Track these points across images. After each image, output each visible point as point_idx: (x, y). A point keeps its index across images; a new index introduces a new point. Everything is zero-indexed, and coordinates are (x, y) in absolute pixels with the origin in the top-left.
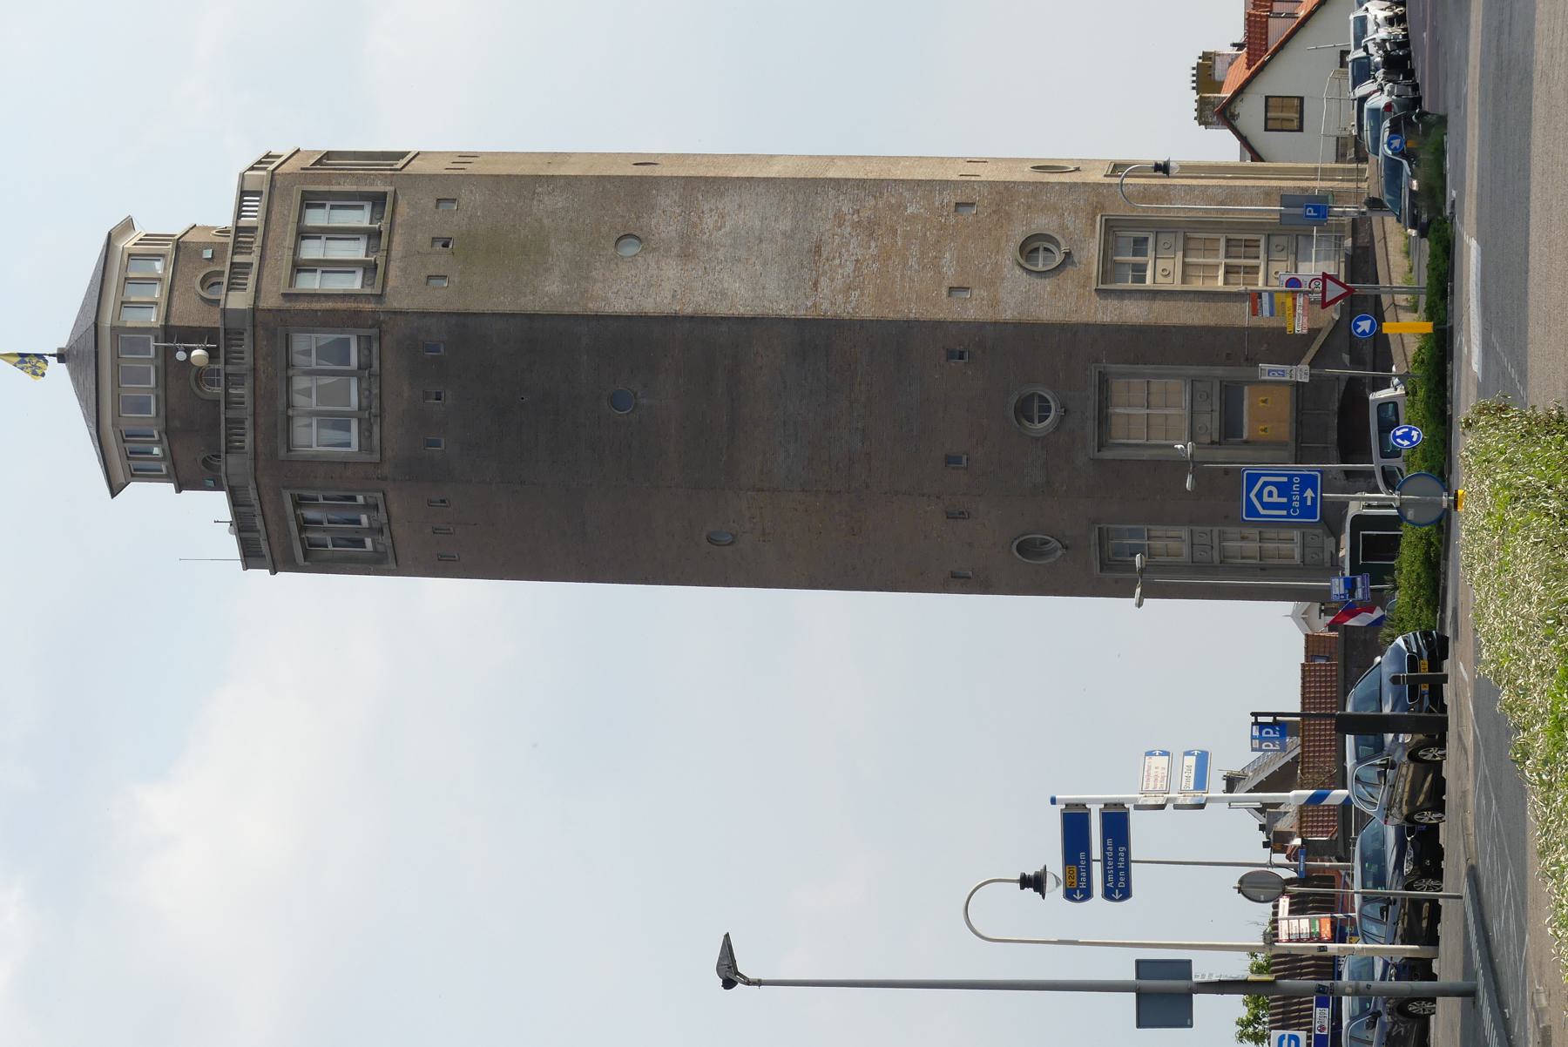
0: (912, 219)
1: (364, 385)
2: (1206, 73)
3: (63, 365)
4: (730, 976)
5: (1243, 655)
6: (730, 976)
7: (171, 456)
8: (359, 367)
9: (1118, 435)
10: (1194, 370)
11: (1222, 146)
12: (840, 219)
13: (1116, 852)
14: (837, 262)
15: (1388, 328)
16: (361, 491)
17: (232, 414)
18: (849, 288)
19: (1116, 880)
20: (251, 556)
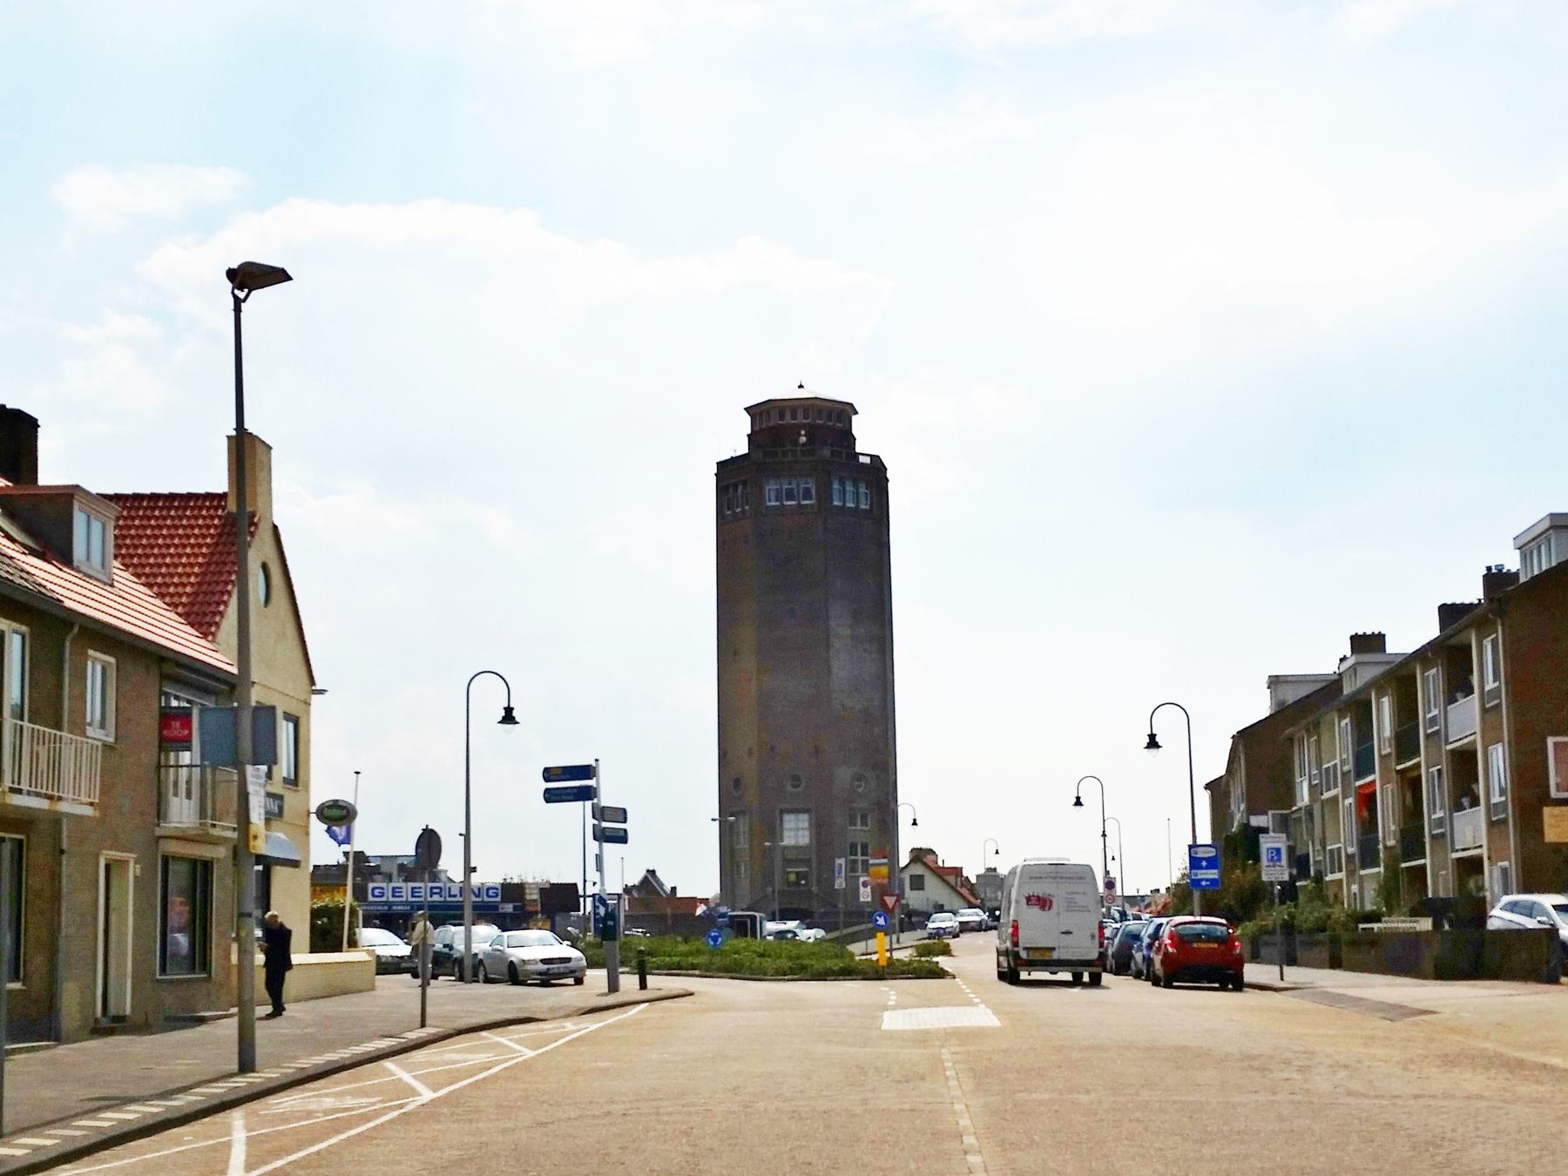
2: (931, 852)
4: (250, 277)
5: (696, 875)
6: (250, 277)
7: (762, 430)
10: (1304, 722)
11: (904, 859)
15: (880, 935)
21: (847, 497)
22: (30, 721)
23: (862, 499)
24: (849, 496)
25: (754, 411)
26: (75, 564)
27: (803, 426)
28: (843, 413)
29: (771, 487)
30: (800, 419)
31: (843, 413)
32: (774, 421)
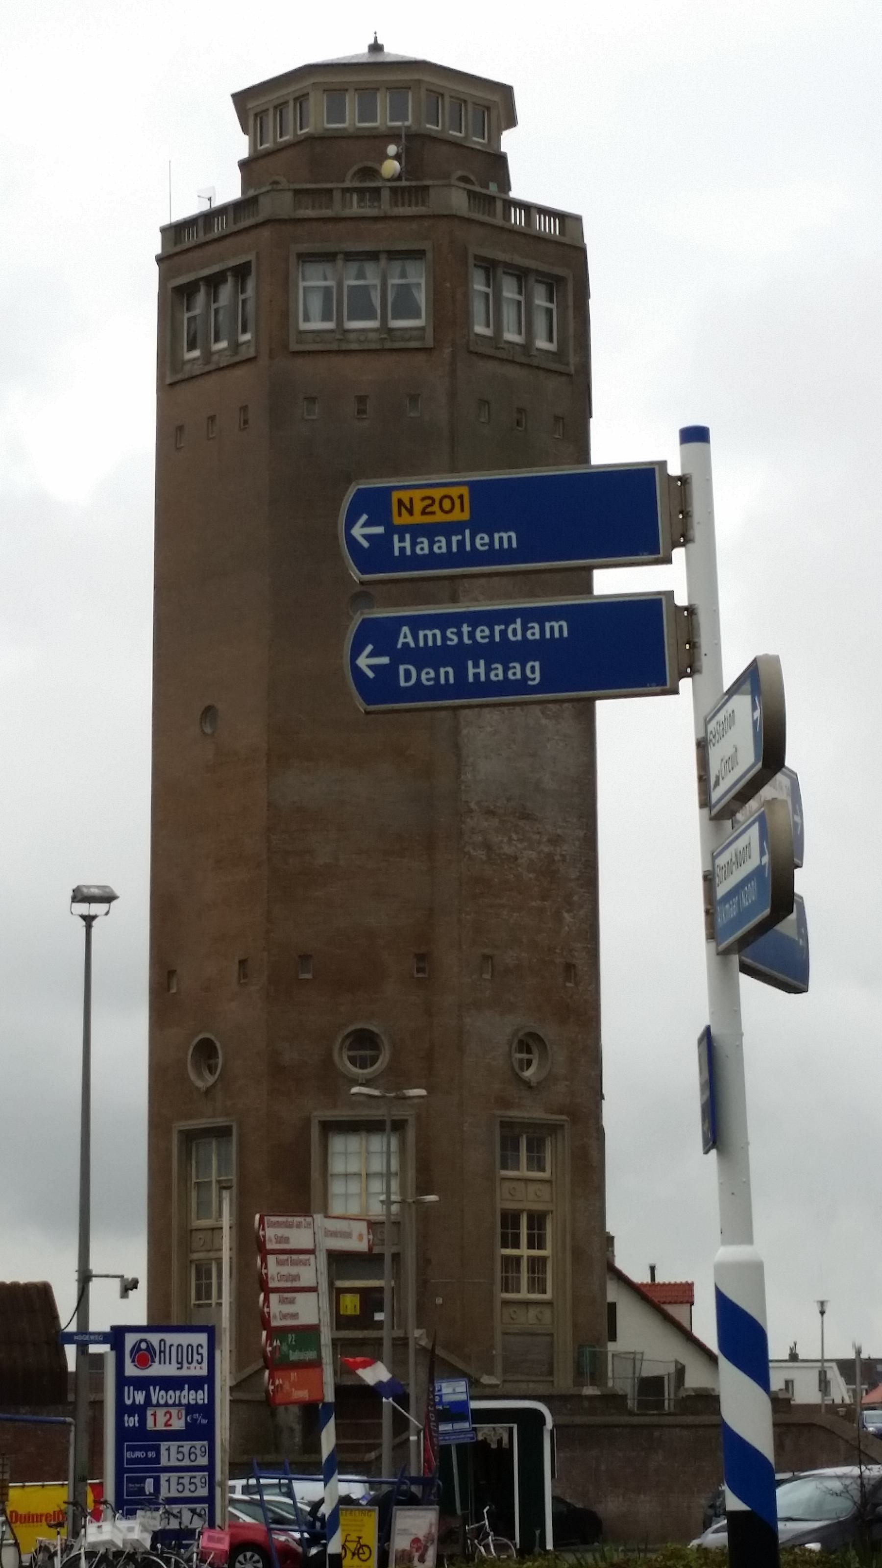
0: (558, 917)
1: (372, 335)
3: (366, 50)
8: (391, 330)
9: (338, 1143)
12: (556, 840)
13: (524, 651)
14: (514, 837)
16: (256, 336)
17: (337, 196)
18: (488, 847)
19: (424, 657)
20: (174, 233)
21: (503, 317)
22: (534, 1234)
23: (540, 324)
24: (509, 315)
25: (253, 105)
26: (466, 192)
27: (393, 136)
28: (494, 104)
29: (313, 281)
30: (382, 121)
31: (494, 104)
32: (318, 120)
